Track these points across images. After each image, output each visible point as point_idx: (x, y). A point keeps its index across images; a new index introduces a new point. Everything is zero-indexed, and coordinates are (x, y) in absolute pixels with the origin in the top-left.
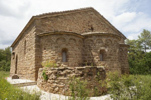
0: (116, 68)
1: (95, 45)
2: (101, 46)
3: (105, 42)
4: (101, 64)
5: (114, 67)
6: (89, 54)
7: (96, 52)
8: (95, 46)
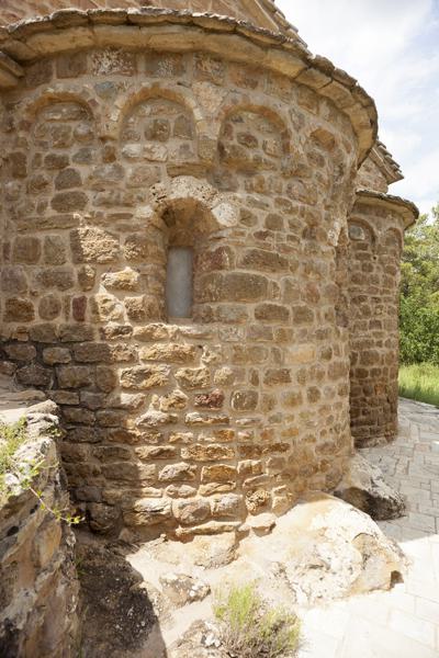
0: (302, 381)
1: (110, 157)
2: (176, 171)
3: (217, 127)
4: (160, 346)
5: (284, 377)
6: (49, 241)
7: (117, 222)
8: (108, 168)
